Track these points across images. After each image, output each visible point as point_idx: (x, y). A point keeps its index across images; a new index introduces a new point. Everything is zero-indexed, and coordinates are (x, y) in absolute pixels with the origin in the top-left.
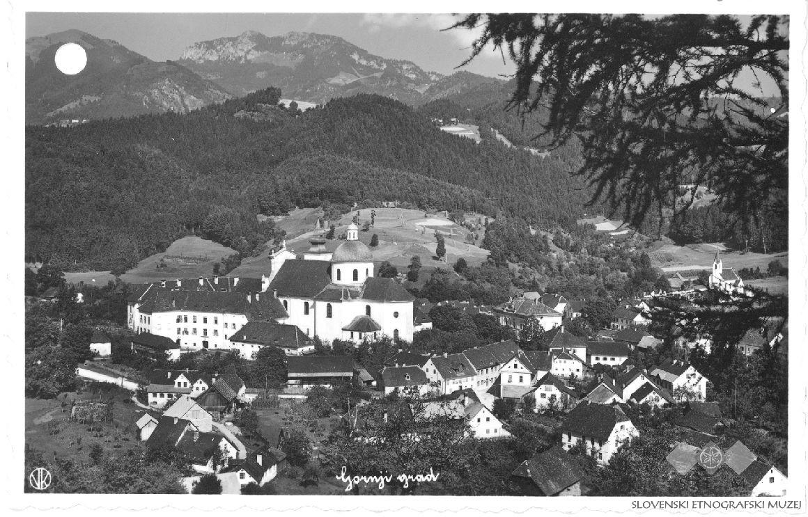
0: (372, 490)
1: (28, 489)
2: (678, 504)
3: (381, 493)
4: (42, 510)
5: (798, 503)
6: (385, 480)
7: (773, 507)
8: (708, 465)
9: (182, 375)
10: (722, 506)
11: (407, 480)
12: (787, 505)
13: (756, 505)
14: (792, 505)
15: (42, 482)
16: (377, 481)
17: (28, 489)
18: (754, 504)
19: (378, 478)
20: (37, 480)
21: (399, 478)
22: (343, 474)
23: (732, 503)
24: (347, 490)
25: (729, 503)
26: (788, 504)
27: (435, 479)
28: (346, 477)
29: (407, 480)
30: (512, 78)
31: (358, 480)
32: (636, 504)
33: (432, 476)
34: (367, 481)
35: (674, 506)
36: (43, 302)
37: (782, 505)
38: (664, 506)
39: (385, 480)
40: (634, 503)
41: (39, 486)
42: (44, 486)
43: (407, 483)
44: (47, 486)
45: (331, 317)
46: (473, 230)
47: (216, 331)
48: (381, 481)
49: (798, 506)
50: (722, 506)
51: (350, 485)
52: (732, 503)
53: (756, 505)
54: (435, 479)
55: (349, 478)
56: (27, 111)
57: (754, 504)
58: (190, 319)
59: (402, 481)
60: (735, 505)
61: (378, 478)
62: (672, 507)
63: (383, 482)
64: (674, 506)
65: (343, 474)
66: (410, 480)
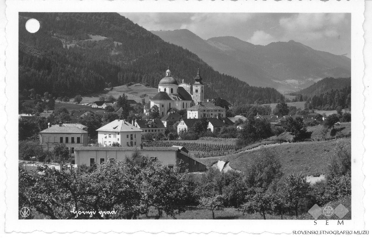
0: (86, 217)
1: (20, 217)
2: (313, 232)
5: (368, 232)
6: (93, 213)
9: (183, 122)
11: (103, 213)
12: (363, 232)
13: (349, 233)
14: (365, 233)
16: (89, 213)
17: (20, 217)
19: (90, 212)
23: (338, 232)
24: (75, 217)
25: (336, 232)
26: (363, 232)
27: (115, 213)
29: (103, 213)
30: (269, 139)
33: (114, 211)
34: (85, 214)
35: (312, 233)
36: (137, 113)
37: (360, 233)
38: (307, 233)
39: (93, 213)
46: (154, 173)
48: (91, 213)
51: (77, 215)
52: (338, 232)
53: (349, 233)
57: (348, 232)
60: (339, 233)
61: (90, 212)
63: (92, 214)
64: (312, 233)
65: (74, 210)
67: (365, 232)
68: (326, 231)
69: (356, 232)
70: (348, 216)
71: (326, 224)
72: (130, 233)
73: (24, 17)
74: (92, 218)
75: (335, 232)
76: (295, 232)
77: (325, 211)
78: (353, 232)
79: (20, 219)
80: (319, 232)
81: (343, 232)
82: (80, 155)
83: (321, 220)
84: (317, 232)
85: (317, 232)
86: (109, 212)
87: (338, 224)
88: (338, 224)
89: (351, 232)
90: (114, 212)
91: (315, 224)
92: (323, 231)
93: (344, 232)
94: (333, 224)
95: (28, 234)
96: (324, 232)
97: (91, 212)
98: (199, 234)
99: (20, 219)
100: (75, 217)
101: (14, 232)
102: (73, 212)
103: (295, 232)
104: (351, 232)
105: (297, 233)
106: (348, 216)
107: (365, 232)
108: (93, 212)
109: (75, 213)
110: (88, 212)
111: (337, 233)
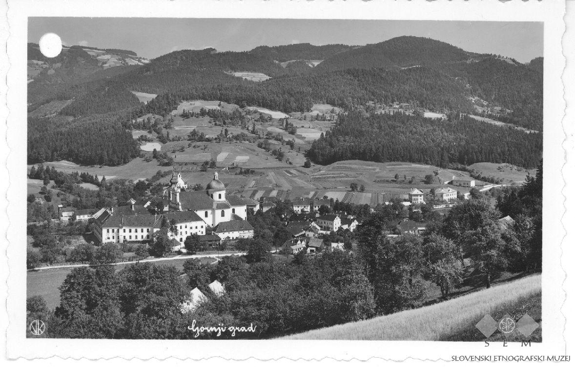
0: (213, 336)
2: (484, 358)
3: (219, 338)
4: (265, 360)
5: (568, 357)
7: (550, 360)
8: (505, 330)
10: (515, 359)
11: (198, 331)
13: (539, 359)
14: (564, 359)
15: (39, 330)
18: (537, 358)
20: (35, 328)
21: (229, 329)
22: (193, 326)
23: (522, 357)
25: (519, 357)
26: (561, 358)
28: (195, 327)
29: (235, 330)
31: (202, 329)
32: (454, 358)
35: (481, 359)
37: (557, 359)
38: (474, 359)
40: (453, 357)
41: (36, 332)
42: (40, 333)
43: (234, 333)
44: (42, 332)
45: (224, 216)
47: (186, 232)
49: (568, 359)
50: (515, 359)
52: (522, 357)
53: (539, 359)
54: (253, 331)
55: (197, 328)
56: (113, 18)
57: (537, 358)
58: (323, 222)
59: (231, 331)
60: (524, 359)
62: (479, 360)
64: (481, 359)
65: (193, 326)
66: (237, 331)
67: (565, 358)
68: (503, 357)
69: (551, 358)
70: (536, 337)
71: (504, 346)
72: (265, 360)
73: (39, 26)
74: (199, 338)
75: (517, 358)
76: (455, 359)
77: (502, 326)
78: (546, 358)
79: (28, 337)
80: (493, 359)
81: (530, 359)
82: (531, 343)
83: (26, 242)
84: (489, 358)
85: (489, 358)
86: (214, 328)
87: (522, 346)
88: (522, 346)
89: (542, 358)
90: (251, 329)
91: (487, 345)
92: (499, 357)
93: (532, 357)
94: (515, 348)
95: (240, 361)
96: (501, 358)
97: (219, 328)
98: (348, 361)
99: (28, 337)
100: (196, 337)
101: (189, 359)
102: (192, 329)
103: (455, 359)
104: (542, 358)
105: (458, 359)
106: (536, 337)
107: (565, 358)
108: (222, 328)
109: (194, 331)
110: (214, 328)
111: (521, 358)
